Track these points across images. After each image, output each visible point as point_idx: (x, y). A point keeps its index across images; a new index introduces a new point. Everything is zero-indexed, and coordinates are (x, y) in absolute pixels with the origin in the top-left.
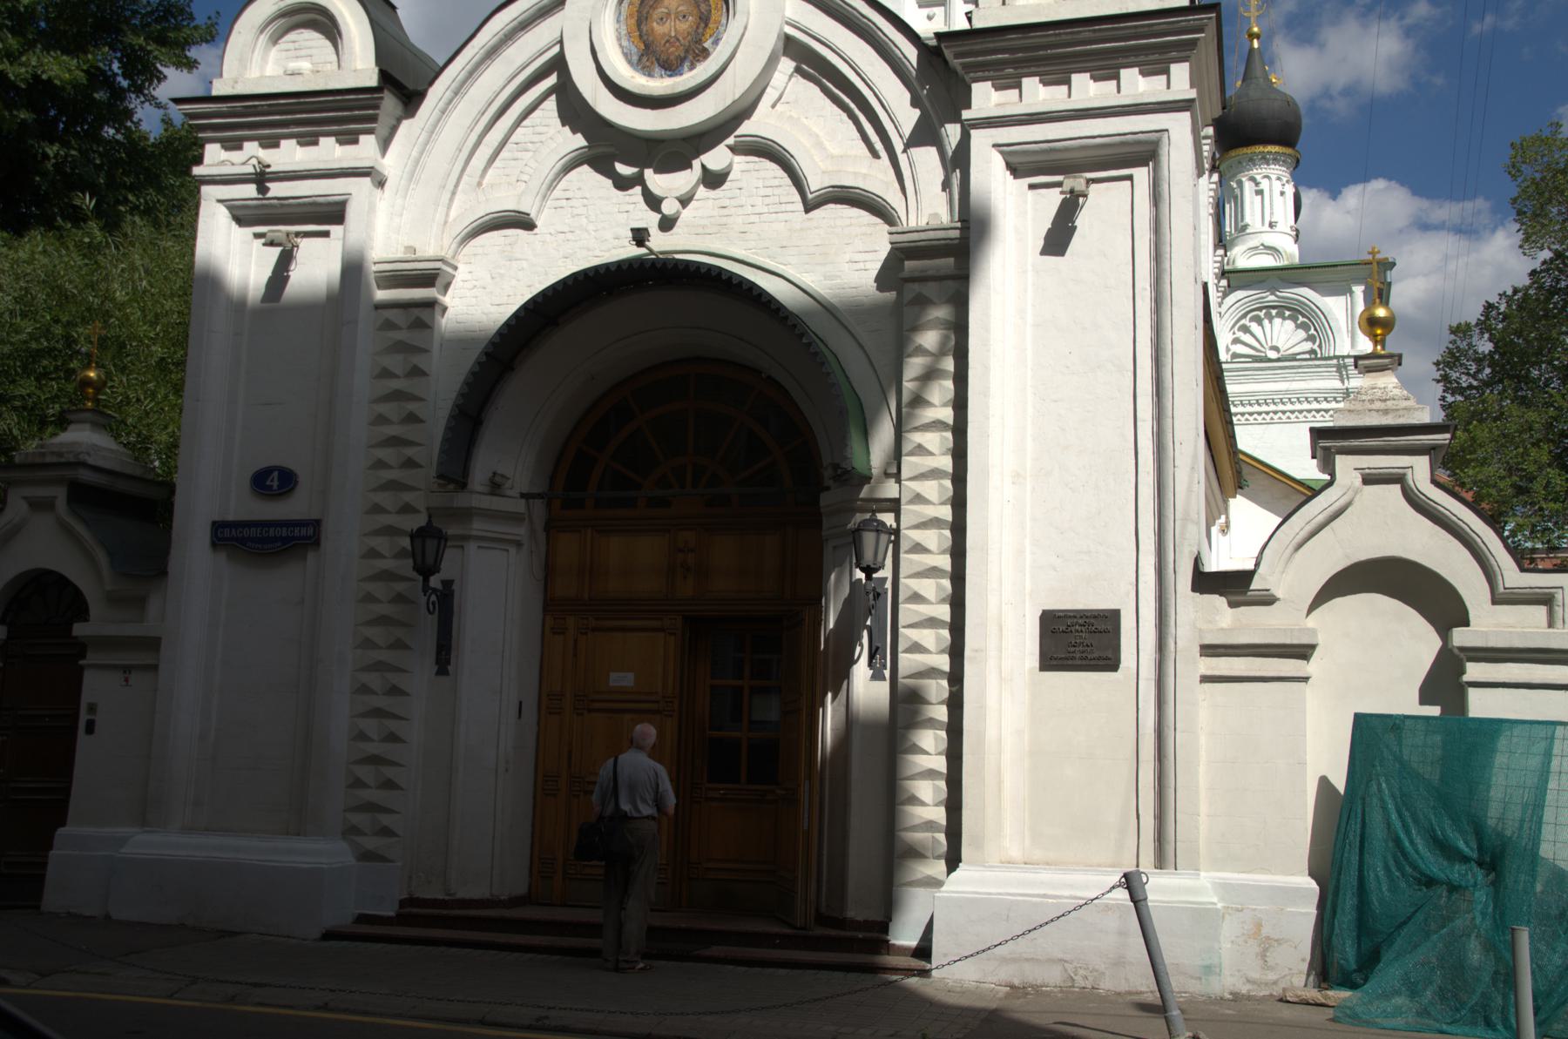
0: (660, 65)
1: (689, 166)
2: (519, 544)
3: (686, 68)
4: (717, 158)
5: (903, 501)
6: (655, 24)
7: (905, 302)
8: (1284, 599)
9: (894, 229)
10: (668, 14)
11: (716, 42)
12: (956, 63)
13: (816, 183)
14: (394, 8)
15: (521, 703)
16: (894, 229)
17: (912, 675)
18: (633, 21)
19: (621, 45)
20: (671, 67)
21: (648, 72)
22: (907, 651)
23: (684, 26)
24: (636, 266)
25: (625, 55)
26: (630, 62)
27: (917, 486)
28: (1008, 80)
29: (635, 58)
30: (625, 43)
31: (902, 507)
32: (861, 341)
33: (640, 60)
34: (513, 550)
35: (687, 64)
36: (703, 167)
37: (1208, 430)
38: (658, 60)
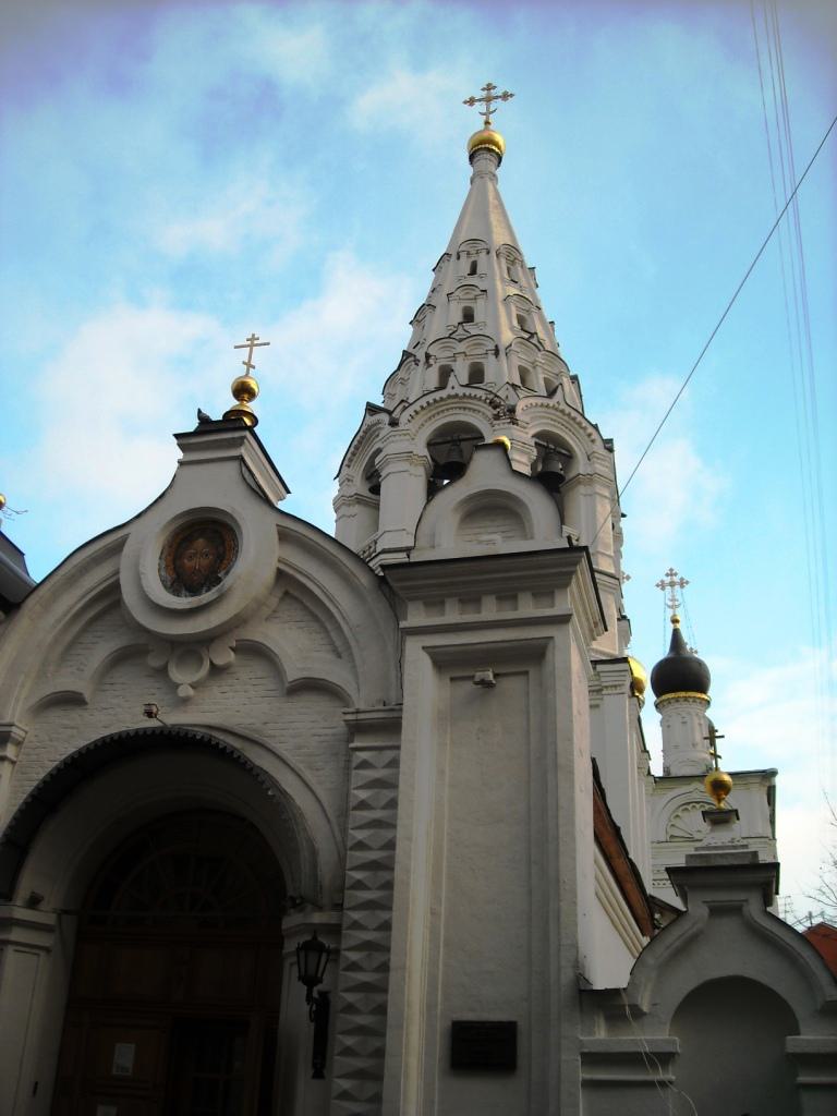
0: (186, 589)
1: (201, 660)
2: (47, 950)
3: (204, 591)
4: (224, 656)
5: (344, 926)
6: (186, 561)
7: (354, 764)
8: (650, 1014)
9: (347, 710)
10: (195, 554)
11: (227, 573)
12: (395, 585)
13: (293, 673)
14: (22, 554)
15: (36, 1083)
16: (347, 710)
17: (559, 510)
18: (170, 558)
19: (160, 575)
20: (194, 591)
21: (177, 593)
22: (340, 1054)
23: (205, 562)
24: (141, 733)
25: (163, 581)
26: (165, 587)
27: (356, 915)
28: (435, 603)
29: (169, 583)
30: (163, 573)
31: (344, 932)
32: (309, 793)
33: (172, 585)
34: (42, 954)
35: (205, 588)
36: (211, 663)
37: (167, 495)
38: (185, 585)
